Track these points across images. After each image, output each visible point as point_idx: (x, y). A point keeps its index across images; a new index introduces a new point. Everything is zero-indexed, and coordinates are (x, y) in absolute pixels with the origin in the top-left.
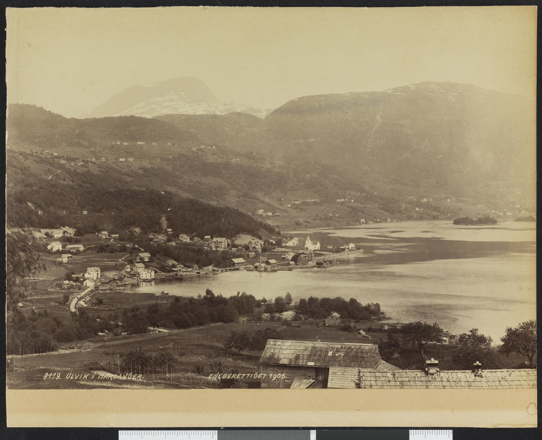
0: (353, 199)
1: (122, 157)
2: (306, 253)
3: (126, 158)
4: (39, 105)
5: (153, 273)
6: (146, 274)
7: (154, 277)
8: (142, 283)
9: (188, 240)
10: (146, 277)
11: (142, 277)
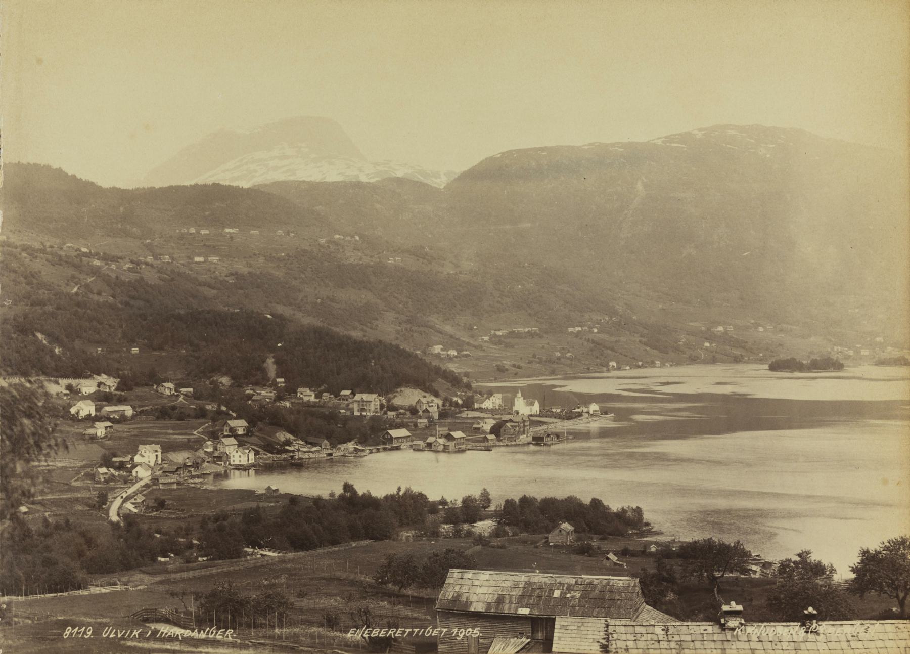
1: (199, 255)
3: (206, 256)
6: (240, 457)
7: (253, 461)
8: (234, 473)
9: (313, 399)
10: (240, 461)
11: (233, 461)
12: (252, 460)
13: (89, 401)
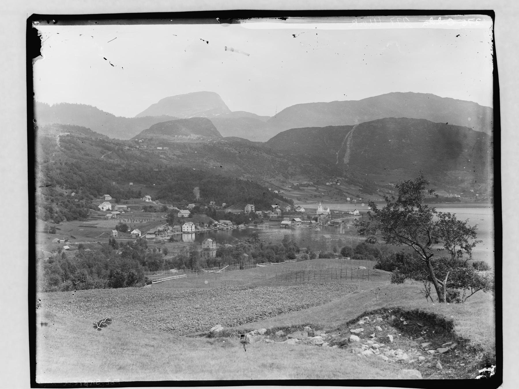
0: (339, 183)
1: (160, 146)
2: (325, 214)
3: (163, 147)
4: (93, 106)
5: (193, 227)
6: (188, 227)
7: (194, 230)
8: (184, 236)
9: (277, 192)
10: (188, 230)
11: (184, 230)
12: (194, 229)
13: (109, 202)
